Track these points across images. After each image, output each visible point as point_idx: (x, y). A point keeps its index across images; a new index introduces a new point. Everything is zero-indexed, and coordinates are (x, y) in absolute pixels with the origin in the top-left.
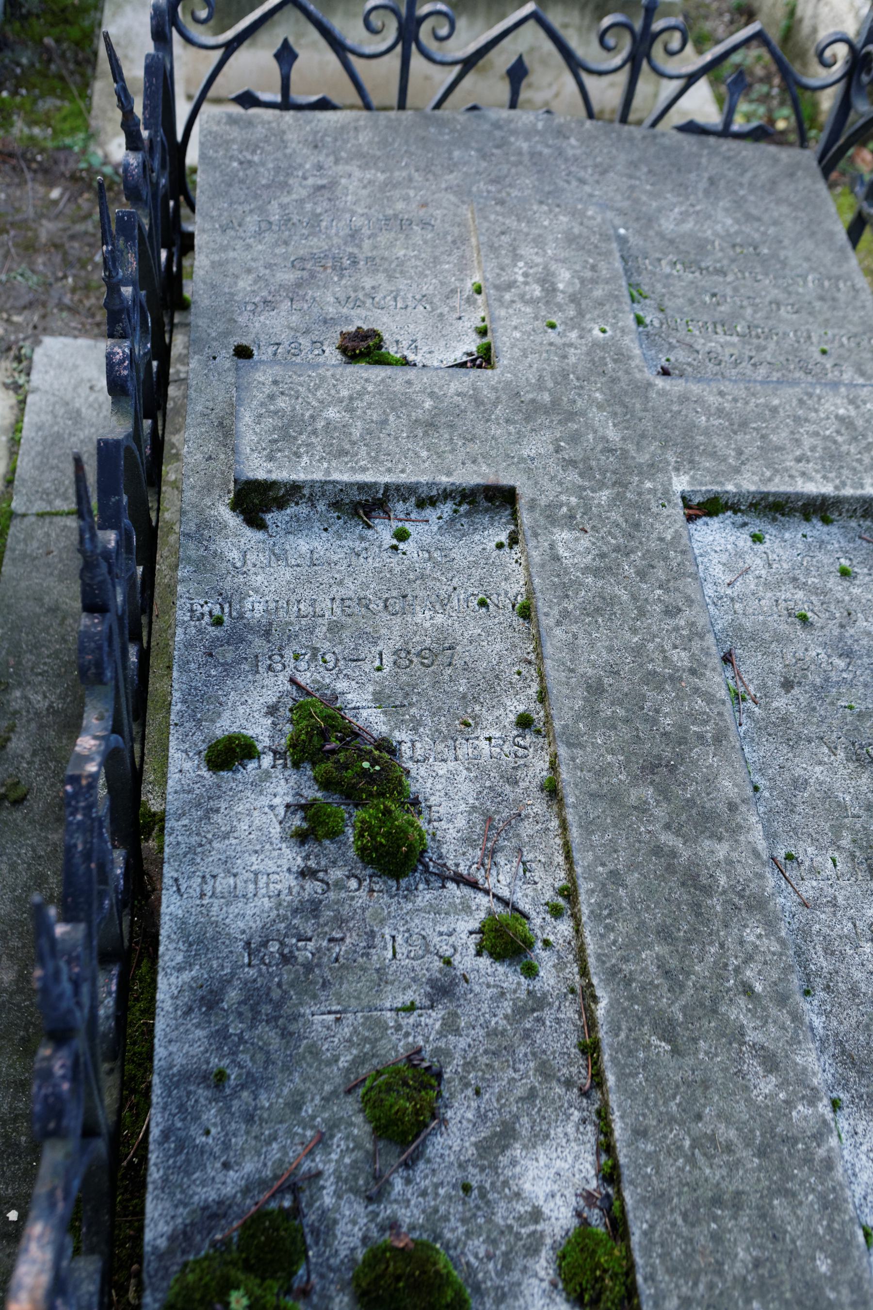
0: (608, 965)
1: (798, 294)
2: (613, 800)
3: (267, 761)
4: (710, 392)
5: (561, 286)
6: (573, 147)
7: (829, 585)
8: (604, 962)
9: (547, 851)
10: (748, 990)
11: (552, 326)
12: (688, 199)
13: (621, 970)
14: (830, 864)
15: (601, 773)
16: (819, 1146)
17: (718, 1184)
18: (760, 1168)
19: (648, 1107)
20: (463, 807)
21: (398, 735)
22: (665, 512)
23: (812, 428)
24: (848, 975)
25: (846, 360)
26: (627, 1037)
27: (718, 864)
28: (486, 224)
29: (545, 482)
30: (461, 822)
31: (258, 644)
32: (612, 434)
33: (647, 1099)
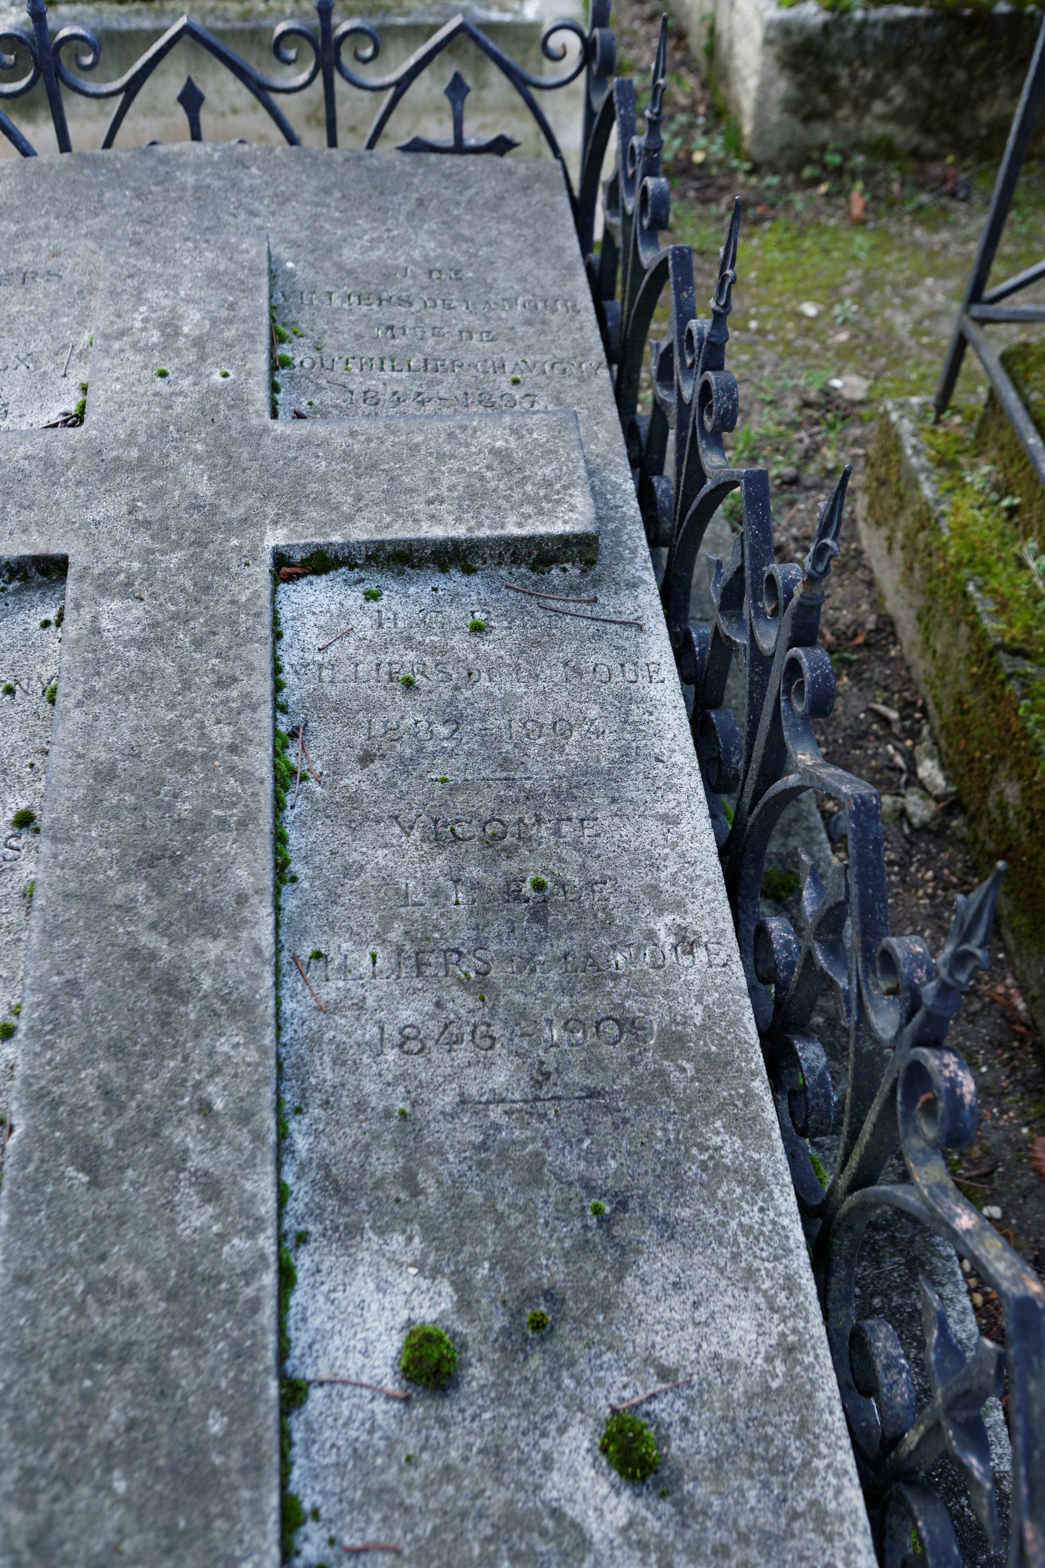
0: (35, 1088)
1: (500, 319)
2: (93, 899)
4: (341, 433)
5: (186, 330)
6: (252, 177)
7: (452, 643)
8: (30, 1085)
9: (14, 964)
10: (205, 1109)
11: (163, 374)
12: (384, 223)
13: (49, 1093)
14: (367, 961)
15: (88, 869)
16: (247, 1284)
17: (107, 1334)
18: (165, 1314)
19: (41, 1249)
22: (247, 571)
23: (455, 465)
24: (357, 1087)
25: (541, 388)
26: (37, 1169)
27: (205, 966)
28: (112, 268)
29: (106, 548)
32: (205, 488)
33: (43, 1239)
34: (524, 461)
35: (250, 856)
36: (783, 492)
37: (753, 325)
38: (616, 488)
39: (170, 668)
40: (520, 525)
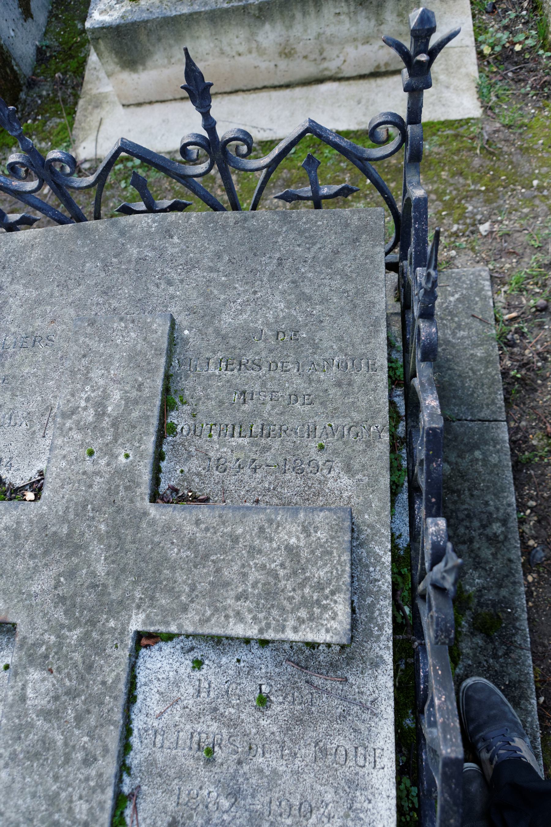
1: (319, 381)
6: (174, 245)
34: (308, 561)
36: (536, 317)
37: (535, 183)
38: (377, 558)
39: (59, 739)
40: (295, 630)
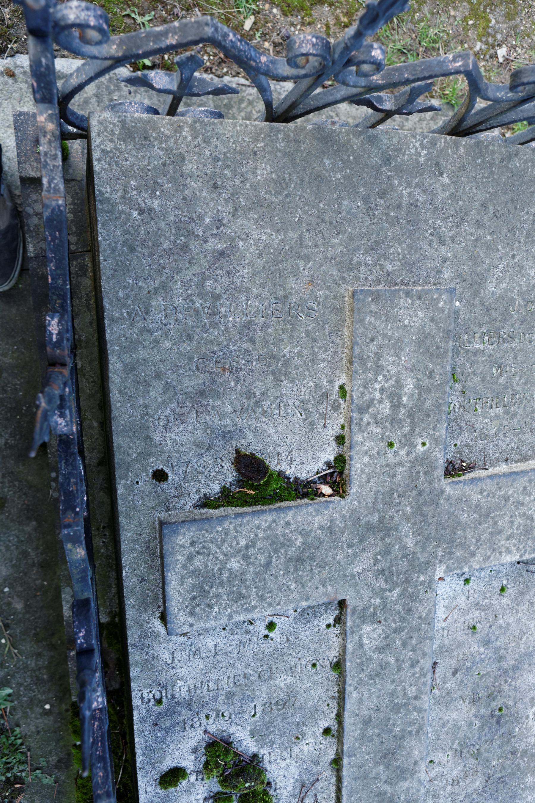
3: (193, 778)
15: (363, 765)
20: (292, 780)
21: (262, 751)
30: (290, 788)
31: (185, 713)
32: (410, 542)
35: (420, 745)
